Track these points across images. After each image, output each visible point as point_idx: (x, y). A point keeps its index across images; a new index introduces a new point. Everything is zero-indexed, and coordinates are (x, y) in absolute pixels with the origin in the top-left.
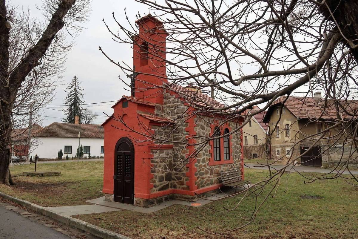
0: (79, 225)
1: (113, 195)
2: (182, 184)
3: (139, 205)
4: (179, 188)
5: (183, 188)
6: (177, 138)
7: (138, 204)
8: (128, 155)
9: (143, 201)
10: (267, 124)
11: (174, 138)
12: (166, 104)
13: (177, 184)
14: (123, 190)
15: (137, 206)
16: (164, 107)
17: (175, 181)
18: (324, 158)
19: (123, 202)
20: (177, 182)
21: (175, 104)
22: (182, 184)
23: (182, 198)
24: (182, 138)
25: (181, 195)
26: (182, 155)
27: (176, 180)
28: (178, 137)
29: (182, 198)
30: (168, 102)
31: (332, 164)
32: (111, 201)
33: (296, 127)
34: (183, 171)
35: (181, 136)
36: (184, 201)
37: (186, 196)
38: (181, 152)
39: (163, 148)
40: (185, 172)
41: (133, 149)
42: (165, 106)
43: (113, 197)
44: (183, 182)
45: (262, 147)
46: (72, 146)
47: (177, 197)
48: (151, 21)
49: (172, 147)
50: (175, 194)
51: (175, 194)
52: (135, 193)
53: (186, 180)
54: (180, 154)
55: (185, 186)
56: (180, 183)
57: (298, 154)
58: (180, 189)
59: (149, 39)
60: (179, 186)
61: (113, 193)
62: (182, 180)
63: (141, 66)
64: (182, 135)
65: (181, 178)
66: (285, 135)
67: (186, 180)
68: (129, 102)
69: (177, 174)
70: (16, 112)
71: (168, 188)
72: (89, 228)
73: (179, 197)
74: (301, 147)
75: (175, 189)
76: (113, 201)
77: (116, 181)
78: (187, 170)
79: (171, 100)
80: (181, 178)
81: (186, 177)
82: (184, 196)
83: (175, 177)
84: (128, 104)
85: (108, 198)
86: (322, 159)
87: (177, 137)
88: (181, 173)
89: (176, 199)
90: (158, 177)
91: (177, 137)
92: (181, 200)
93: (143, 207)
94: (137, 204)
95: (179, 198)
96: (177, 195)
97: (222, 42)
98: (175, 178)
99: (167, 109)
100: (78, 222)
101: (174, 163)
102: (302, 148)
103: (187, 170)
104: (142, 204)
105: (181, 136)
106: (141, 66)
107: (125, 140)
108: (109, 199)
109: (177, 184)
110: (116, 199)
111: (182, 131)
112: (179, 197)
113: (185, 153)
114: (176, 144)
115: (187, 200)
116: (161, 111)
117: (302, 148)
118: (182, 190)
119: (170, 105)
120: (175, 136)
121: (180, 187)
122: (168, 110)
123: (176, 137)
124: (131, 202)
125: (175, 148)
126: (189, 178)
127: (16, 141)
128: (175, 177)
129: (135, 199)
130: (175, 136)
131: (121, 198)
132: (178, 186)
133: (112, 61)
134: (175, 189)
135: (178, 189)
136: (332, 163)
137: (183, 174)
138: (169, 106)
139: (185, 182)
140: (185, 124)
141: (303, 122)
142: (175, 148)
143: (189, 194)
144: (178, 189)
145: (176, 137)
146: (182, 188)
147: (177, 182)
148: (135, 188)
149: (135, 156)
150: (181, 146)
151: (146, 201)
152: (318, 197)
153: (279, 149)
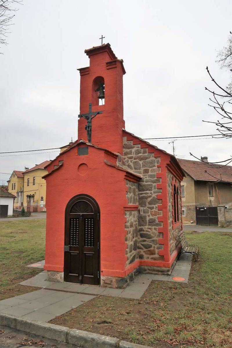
1: (63, 274)
2: (152, 253)
3: (110, 286)
4: (147, 259)
5: (154, 259)
6: (144, 196)
7: (107, 285)
9: (117, 280)
11: (139, 196)
12: (126, 154)
13: (144, 254)
14: (81, 264)
15: (106, 287)
16: (124, 159)
17: (141, 250)
18: (221, 218)
19: (82, 282)
20: (145, 252)
21: (140, 155)
22: (152, 253)
23: (154, 270)
24: (151, 196)
25: (152, 267)
26: (151, 217)
27: (142, 249)
28: (146, 195)
29: (154, 270)
30: (131, 153)
31: (228, 223)
32: (58, 282)
33: (193, 188)
34: (154, 237)
35: (151, 195)
36: (156, 274)
37: (159, 269)
38: (150, 214)
39: (131, 209)
40: (155, 238)
41: (98, 211)
42: (126, 157)
43: (63, 276)
44: (154, 250)
46: (8, 205)
47: (146, 270)
48: (108, 52)
49: (137, 208)
50: (143, 267)
51: (143, 267)
53: (158, 248)
54: (149, 216)
55: (156, 256)
56: (149, 253)
57: (194, 215)
58: (149, 260)
59: (102, 73)
60: (148, 256)
61: (63, 270)
62: (152, 249)
64: (151, 193)
65: (150, 246)
67: (158, 248)
68: (89, 148)
69: (144, 241)
73: (149, 270)
74: (196, 208)
75: (143, 260)
76: (62, 280)
78: (159, 236)
79: (133, 150)
80: (150, 246)
81: (158, 245)
82: (156, 268)
83: (142, 245)
84: (89, 150)
85: (54, 277)
86: (219, 219)
87: (144, 195)
88: (151, 239)
89: (144, 272)
90: (129, 247)
91: (144, 195)
92: (151, 273)
93: (117, 288)
94: (106, 285)
95: (148, 271)
96: (146, 268)
98: (142, 246)
99: (128, 161)
101: (140, 227)
102: (198, 209)
103: (159, 236)
104: (115, 285)
105: (151, 195)
107: (80, 199)
108: (56, 279)
109: (144, 254)
110: (67, 278)
111: (152, 188)
112: (149, 270)
113: (156, 215)
114: (142, 204)
115: (160, 273)
116: (121, 163)
117: (198, 209)
118: (153, 261)
119: (134, 155)
120: (141, 194)
121: (148, 258)
122: (130, 162)
123: (142, 195)
124: (96, 281)
125: (141, 208)
126: (163, 246)
128: (142, 245)
129: (102, 278)
130: (141, 194)
131: (79, 276)
132: (145, 256)
133: (213, 80)
134: (143, 260)
135: (145, 259)
136: (228, 222)
137: (153, 241)
138: (131, 158)
139: (157, 251)
140: (156, 180)
141: (199, 184)
142: (141, 208)
143: (164, 266)
144: (145, 259)
145: (142, 195)
146: (152, 258)
147: (145, 252)
148: (101, 262)
149: (101, 220)
150: (150, 206)
151: (121, 280)
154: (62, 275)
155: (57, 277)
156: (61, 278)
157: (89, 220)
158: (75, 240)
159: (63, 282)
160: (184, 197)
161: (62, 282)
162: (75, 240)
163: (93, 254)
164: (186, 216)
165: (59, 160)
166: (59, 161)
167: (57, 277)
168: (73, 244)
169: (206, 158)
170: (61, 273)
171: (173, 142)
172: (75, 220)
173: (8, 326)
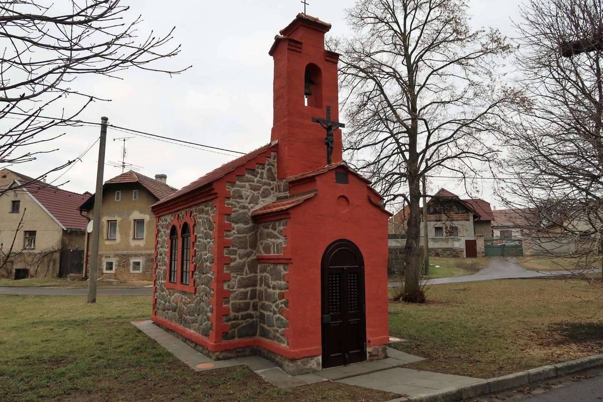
0: (547, 372)
1: (320, 358)
3: (376, 358)
8: (357, 276)
10: (84, 213)
19: (345, 363)
32: (315, 372)
45: (47, 255)
52: (368, 337)
63: (322, 109)
66: (131, 237)
70: (404, 188)
71: (255, 335)
72: (561, 369)
77: (325, 327)
85: (308, 366)
94: (372, 358)
97: (587, 146)
100: (543, 371)
106: (322, 109)
107: (338, 246)
108: (311, 368)
127: (587, 253)
129: (369, 350)
152: (171, 330)
153: (114, 261)
154: (319, 359)
155: (311, 365)
156: (318, 364)
157: (338, 276)
158: (335, 305)
159: (321, 369)
160: (143, 239)
161: (319, 371)
162: (335, 305)
163: (340, 323)
164: (143, 272)
165: (237, 174)
166: (237, 176)
167: (311, 365)
168: (333, 312)
169: (164, 177)
170: (316, 358)
171: (124, 140)
172: (334, 276)
173: (482, 394)
